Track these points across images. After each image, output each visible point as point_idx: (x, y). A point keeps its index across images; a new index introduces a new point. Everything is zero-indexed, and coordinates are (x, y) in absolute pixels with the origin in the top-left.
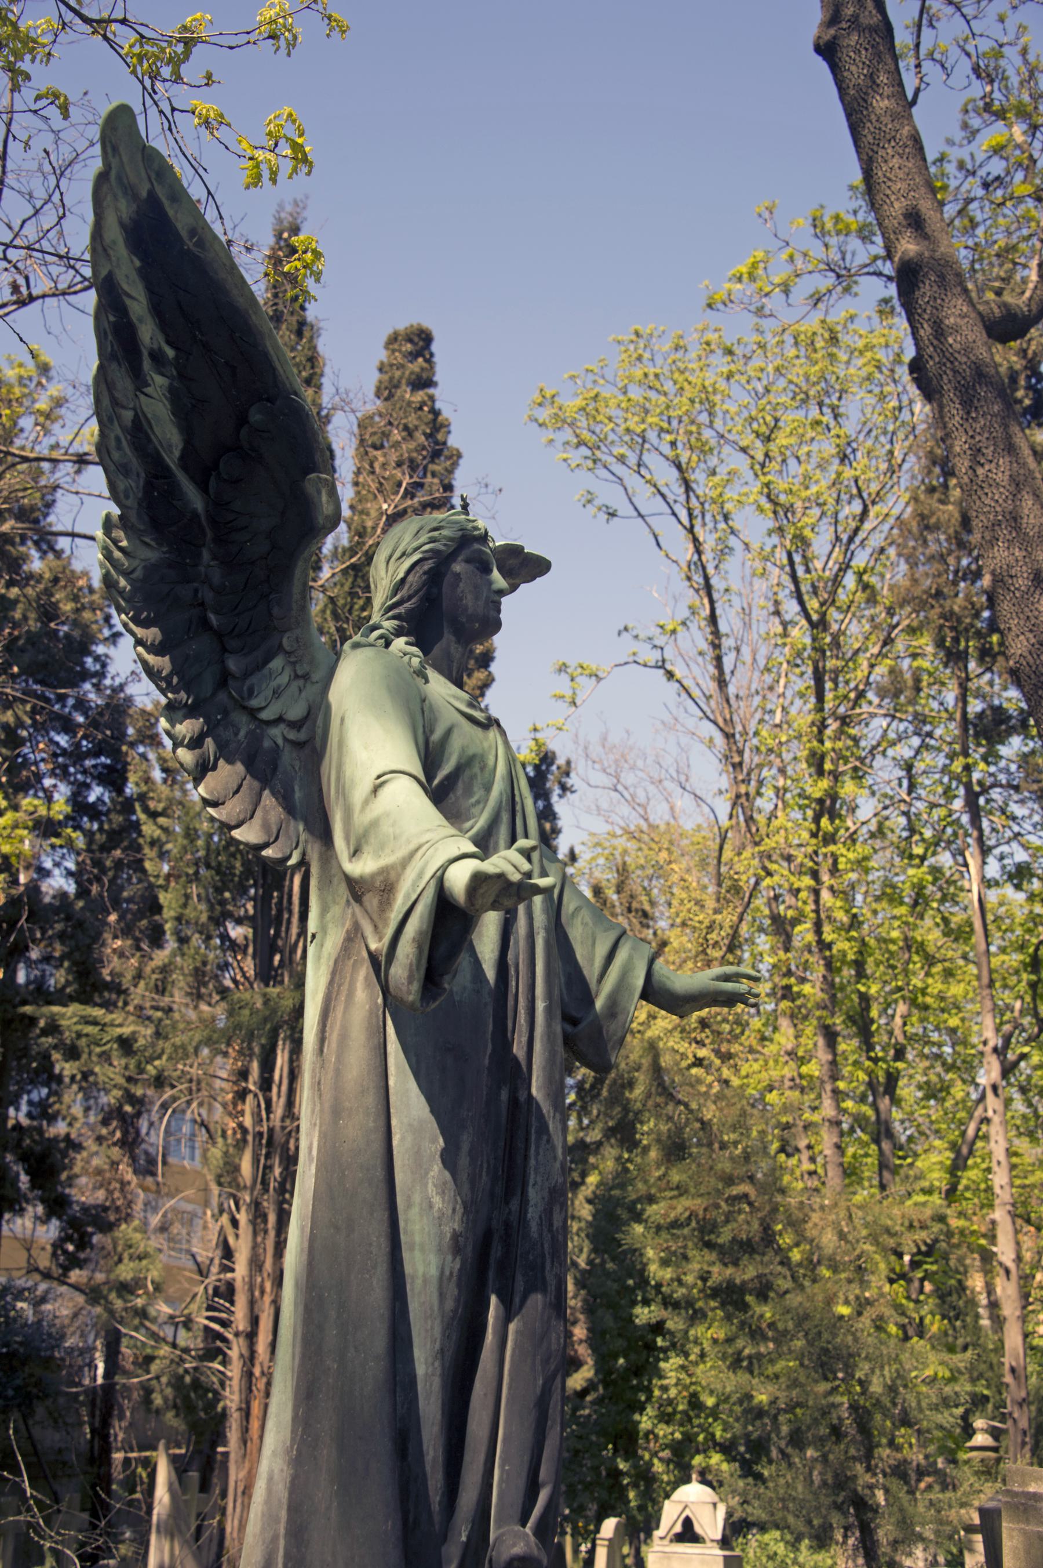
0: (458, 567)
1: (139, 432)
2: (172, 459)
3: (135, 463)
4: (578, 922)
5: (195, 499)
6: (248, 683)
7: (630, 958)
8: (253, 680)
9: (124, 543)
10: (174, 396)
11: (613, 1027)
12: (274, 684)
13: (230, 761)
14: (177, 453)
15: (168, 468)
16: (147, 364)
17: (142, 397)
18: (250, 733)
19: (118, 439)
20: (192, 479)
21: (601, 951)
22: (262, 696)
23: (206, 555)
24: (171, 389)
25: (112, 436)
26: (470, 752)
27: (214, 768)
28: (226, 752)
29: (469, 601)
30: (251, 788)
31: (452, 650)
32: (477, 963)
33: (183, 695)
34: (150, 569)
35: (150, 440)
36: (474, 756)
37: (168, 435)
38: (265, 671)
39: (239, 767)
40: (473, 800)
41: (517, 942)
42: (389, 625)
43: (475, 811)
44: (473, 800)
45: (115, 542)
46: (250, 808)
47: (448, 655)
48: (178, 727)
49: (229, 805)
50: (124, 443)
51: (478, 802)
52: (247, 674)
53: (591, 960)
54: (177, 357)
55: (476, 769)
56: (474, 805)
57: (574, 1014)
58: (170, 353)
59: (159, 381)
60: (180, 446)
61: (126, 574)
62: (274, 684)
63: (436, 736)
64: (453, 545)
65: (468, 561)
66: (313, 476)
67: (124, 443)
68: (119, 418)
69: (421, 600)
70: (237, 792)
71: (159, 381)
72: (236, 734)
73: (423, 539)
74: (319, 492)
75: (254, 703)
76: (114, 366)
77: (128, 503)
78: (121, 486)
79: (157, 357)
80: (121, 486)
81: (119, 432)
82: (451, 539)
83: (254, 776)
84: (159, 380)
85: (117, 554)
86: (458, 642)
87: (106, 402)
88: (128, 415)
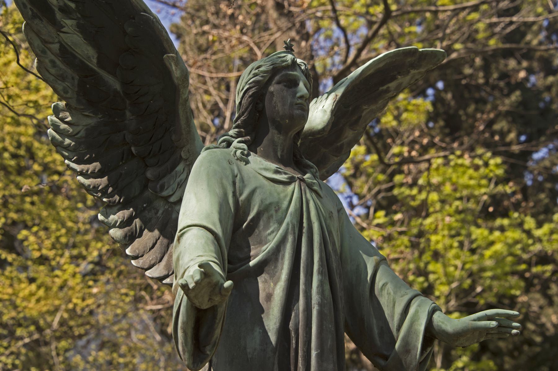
0: (272, 89)
1: (65, 53)
2: (93, 64)
3: (69, 72)
4: (385, 292)
5: (114, 83)
6: (161, 182)
7: (417, 312)
8: (165, 180)
9: (69, 119)
10: (81, 29)
11: (409, 359)
12: (178, 180)
13: (151, 230)
14: (95, 61)
15: (92, 70)
16: (59, 15)
17: (61, 34)
18: (166, 211)
19: (53, 62)
20: (109, 72)
21: (399, 309)
22: (170, 189)
23: (128, 114)
24: (79, 26)
25: (47, 61)
26: (268, 202)
27: (140, 235)
28: (148, 225)
29: (279, 107)
30: (161, 244)
31: (276, 139)
32: (265, 333)
33: (117, 198)
34: (90, 131)
35: (75, 57)
36: (270, 204)
37: (86, 52)
38: (173, 173)
39: (156, 233)
40: (269, 231)
41: (297, 315)
42: (232, 132)
43: (270, 238)
44: (269, 231)
45: (62, 120)
46: (159, 256)
47: (273, 143)
48: (112, 217)
49: (146, 256)
50: (58, 62)
51: (272, 232)
52: (160, 177)
53: (392, 317)
54: (77, 7)
55: (273, 212)
56: (269, 234)
57: (385, 353)
58: (73, 5)
59: (69, 23)
60: (96, 56)
61: (70, 136)
62: (178, 180)
63: (243, 198)
64: (268, 76)
65: (279, 83)
66: (165, 56)
67: (58, 62)
68: (50, 49)
69: (249, 113)
70: (153, 247)
71: (69, 23)
72: (156, 213)
73: (251, 76)
74: (171, 65)
75: (165, 193)
76: (37, 21)
77: (69, 95)
78: (60, 88)
79: (65, 10)
80: (60, 88)
81: (53, 57)
82: (265, 72)
83: (165, 237)
84: (69, 22)
85: (63, 126)
86: (280, 132)
87: (37, 42)
88: (56, 47)
